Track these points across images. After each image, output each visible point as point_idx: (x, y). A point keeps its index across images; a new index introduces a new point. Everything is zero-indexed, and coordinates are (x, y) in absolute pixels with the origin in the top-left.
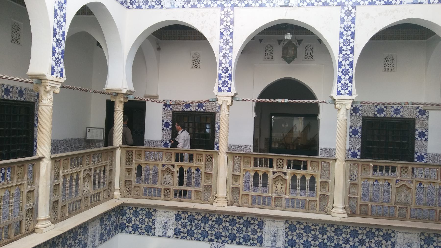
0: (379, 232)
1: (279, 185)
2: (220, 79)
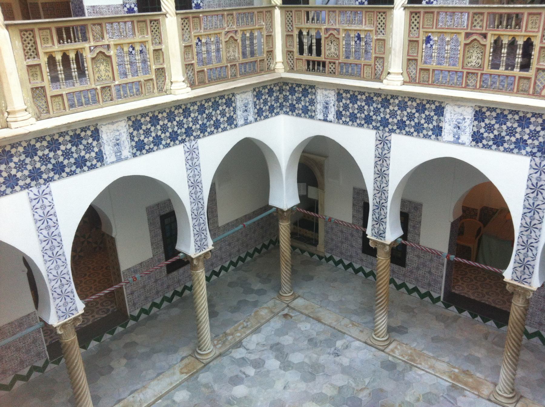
0: (17, 148)
1: (102, 67)
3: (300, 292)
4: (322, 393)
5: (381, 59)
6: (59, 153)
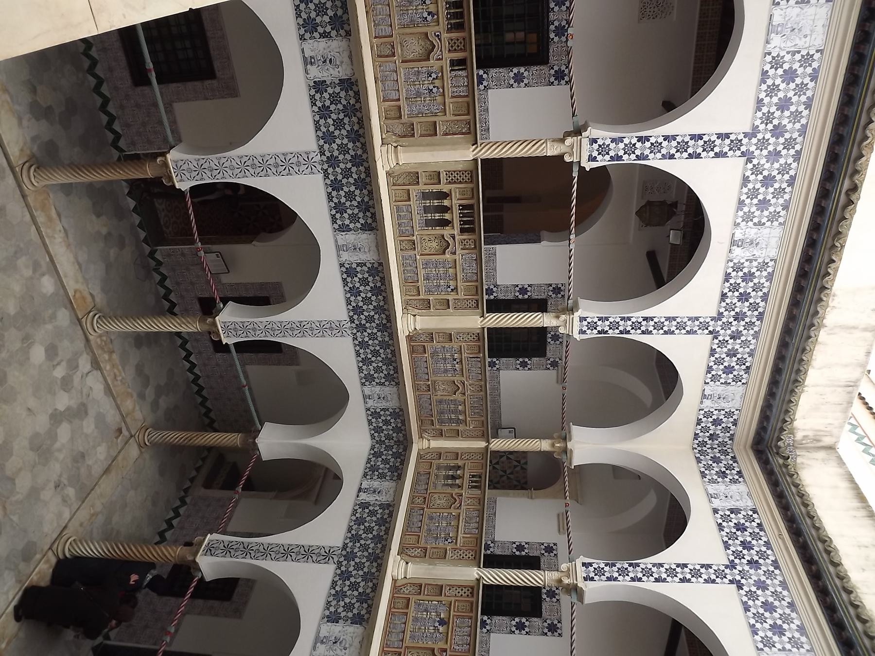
2: (613, 140)
3: (147, 456)
4: (11, 455)
5: (424, 555)
6: (353, 188)
